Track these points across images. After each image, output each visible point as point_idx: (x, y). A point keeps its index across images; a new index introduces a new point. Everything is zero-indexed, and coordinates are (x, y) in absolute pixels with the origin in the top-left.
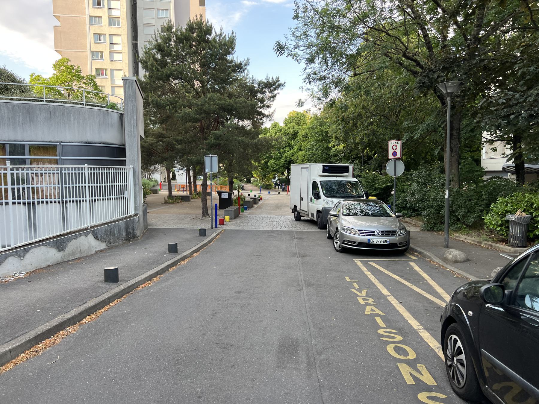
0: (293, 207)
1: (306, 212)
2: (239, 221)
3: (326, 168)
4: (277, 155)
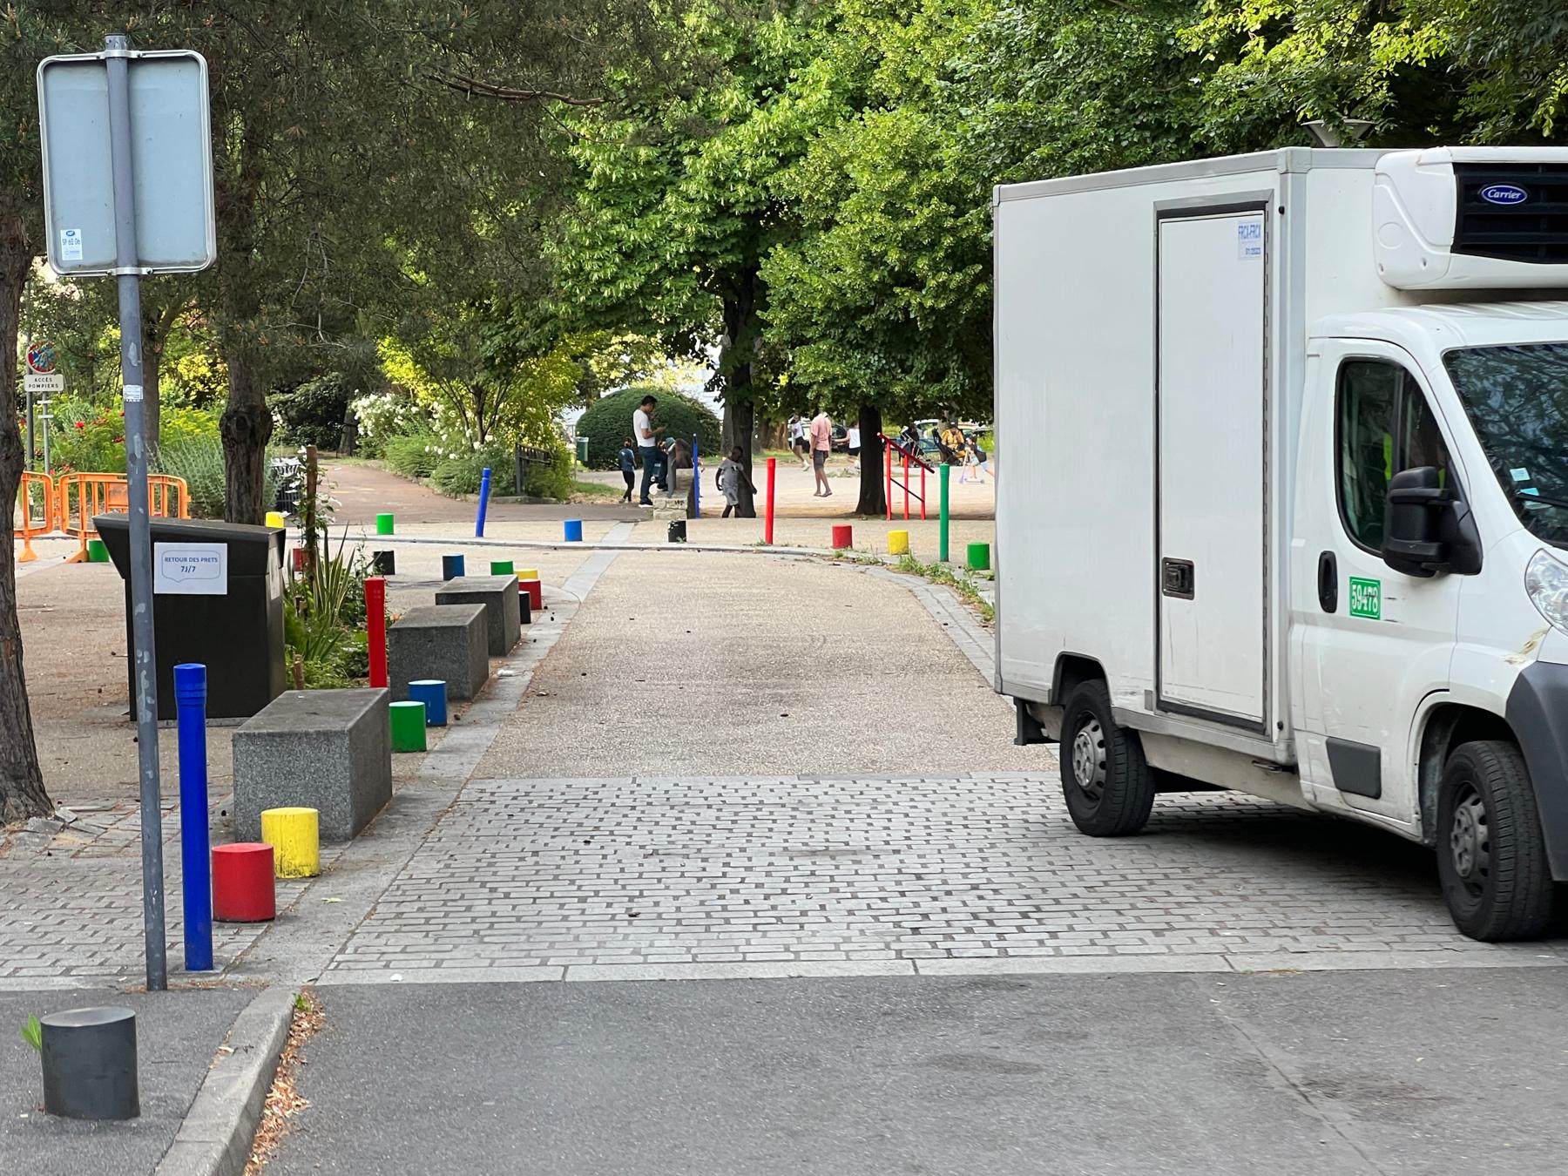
0: (1041, 679)
1: (1258, 729)
2: (427, 867)
3: (1493, 194)
4: (630, 162)
